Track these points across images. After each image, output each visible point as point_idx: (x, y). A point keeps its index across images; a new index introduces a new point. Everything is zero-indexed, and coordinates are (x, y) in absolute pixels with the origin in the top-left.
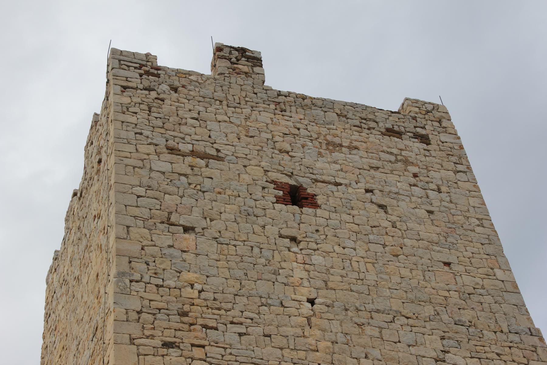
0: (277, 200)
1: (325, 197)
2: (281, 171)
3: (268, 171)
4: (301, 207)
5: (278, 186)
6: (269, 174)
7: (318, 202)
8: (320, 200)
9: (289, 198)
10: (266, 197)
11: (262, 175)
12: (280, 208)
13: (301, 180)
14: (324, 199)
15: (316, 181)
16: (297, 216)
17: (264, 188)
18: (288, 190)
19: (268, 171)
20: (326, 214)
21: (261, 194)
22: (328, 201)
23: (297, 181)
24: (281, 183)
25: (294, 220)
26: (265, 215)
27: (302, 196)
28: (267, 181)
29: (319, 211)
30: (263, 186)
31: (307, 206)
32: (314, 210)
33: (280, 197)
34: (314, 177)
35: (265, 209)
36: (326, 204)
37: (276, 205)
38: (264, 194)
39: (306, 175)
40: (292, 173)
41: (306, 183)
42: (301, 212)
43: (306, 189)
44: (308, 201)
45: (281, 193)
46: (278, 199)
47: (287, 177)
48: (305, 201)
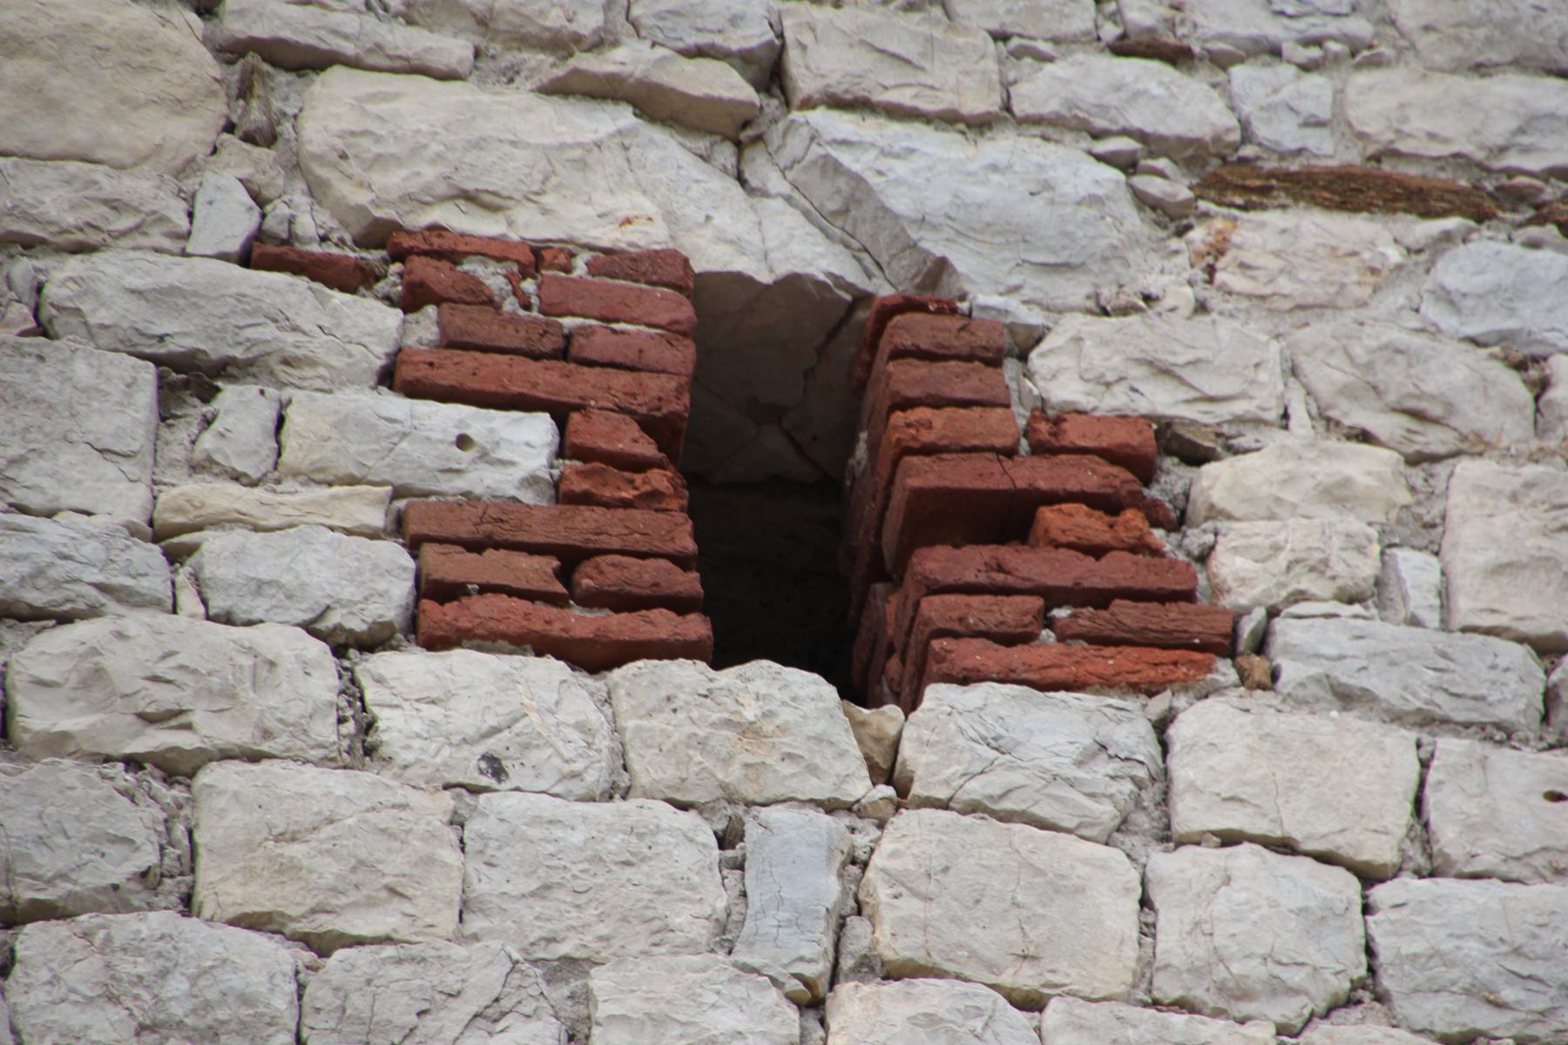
0: (431, 590)
1: (1368, 467)
2: (560, 44)
3: (307, 62)
4: (869, 669)
5: (460, 307)
6: (327, 110)
7: (1229, 565)
8: (1259, 526)
9: (656, 531)
10: (213, 543)
11: (190, 131)
12: (465, 716)
13: (921, 177)
14: (1338, 495)
15: (1236, 176)
16: (797, 856)
17: (189, 380)
18: (664, 390)
19: (307, 62)
20: (1356, 780)
21: (125, 500)
22: (1429, 532)
23: (846, 207)
24: (536, 258)
25: (725, 934)
26: (173, 882)
27: (922, 475)
28: (261, 252)
29: (1217, 731)
30: (182, 333)
31: (1011, 654)
32: (1127, 723)
33: (488, 531)
34: (1186, 105)
35: (176, 769)
36: (1372, 594)
37: (403, 670)
38: (191, 493)
39: (1040, 89)
40: (770, 71)
41: (1011, 234)
42: (887, 769)
43: (1025, 343)
44: (1028, 564)
45: (526, 442)
46: (450, 565)
47: (666, 150)
48: (971, 562)
